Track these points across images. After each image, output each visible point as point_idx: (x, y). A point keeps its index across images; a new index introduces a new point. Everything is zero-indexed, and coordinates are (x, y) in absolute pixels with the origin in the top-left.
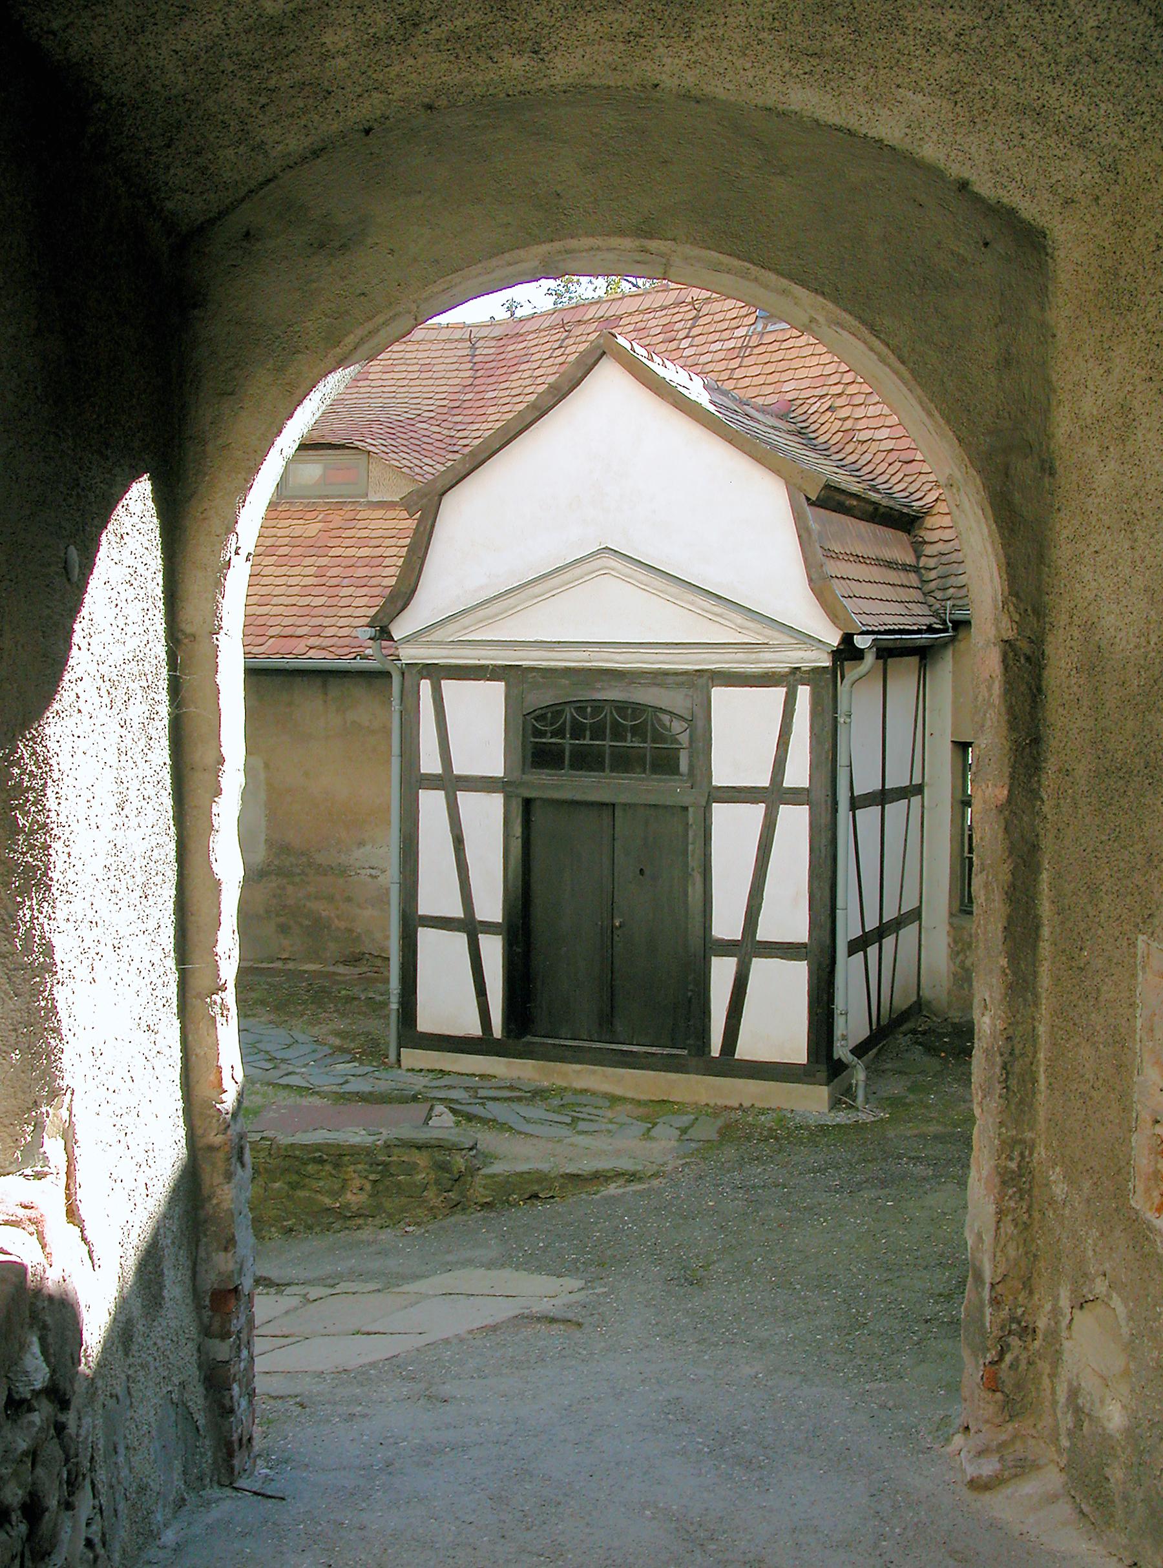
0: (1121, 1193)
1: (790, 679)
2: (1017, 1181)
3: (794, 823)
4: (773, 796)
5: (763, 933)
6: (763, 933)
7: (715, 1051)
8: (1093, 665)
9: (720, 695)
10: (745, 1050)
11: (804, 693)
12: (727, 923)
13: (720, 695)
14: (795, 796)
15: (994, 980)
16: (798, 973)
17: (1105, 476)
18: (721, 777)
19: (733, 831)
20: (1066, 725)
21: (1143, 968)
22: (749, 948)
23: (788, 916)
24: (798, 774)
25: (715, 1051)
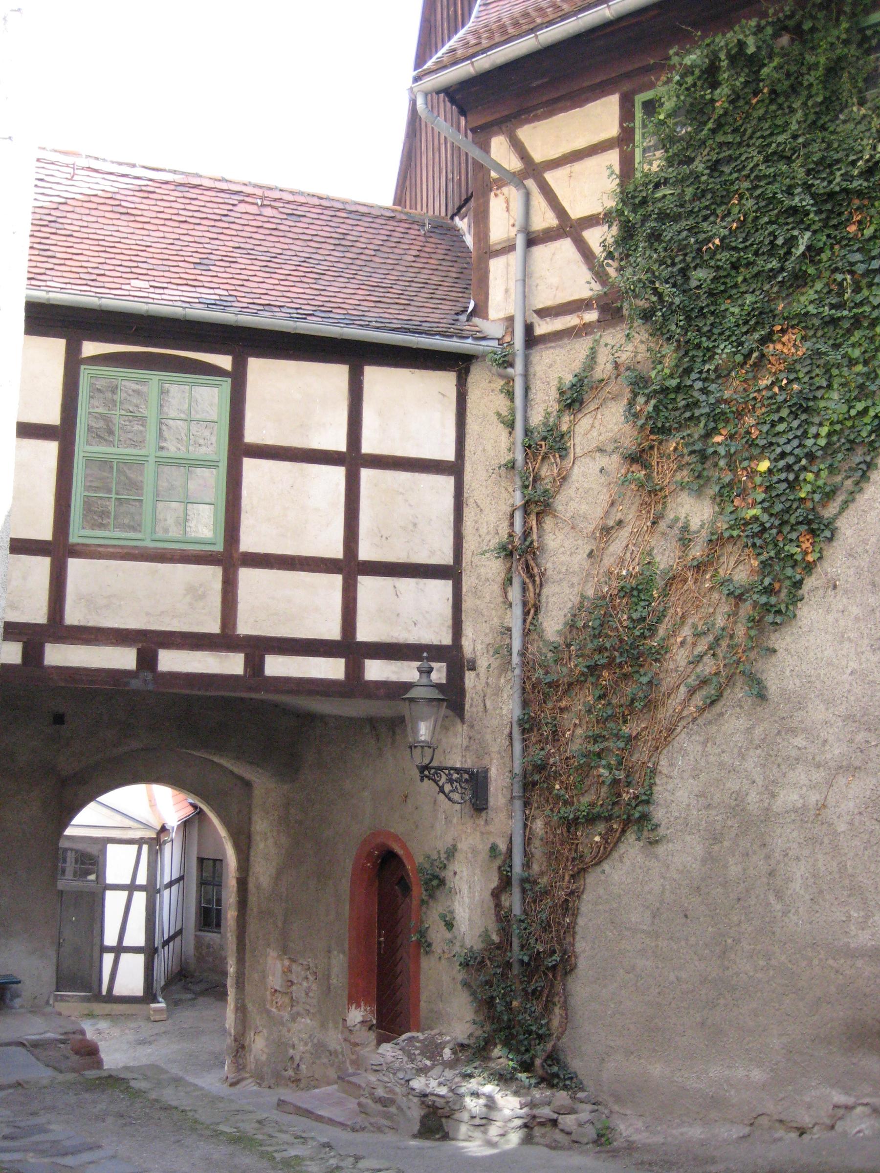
0: (265, 1005)
1: (140, 842)
2: (241, 1009)
3: (140, 898)
4: (131, 888)
5: (126, 943)
6: (126, 943)
7: (104, 992)
8: (258, 887)
9: (110, 847)
10: (118, 991)
11: (145, 848)
12: (110, 939)
13: (110, 847)
14: (141, 888)
15: (742, 1076)
16: (140, 959)
17: (261, 846)
18: (110, 879)
19: (114, 902)
20: (253, 900)
21: (544, 458)
22: (119, 949)
23: (136, 936)
24: (142, 879)
25: (104, 992)
